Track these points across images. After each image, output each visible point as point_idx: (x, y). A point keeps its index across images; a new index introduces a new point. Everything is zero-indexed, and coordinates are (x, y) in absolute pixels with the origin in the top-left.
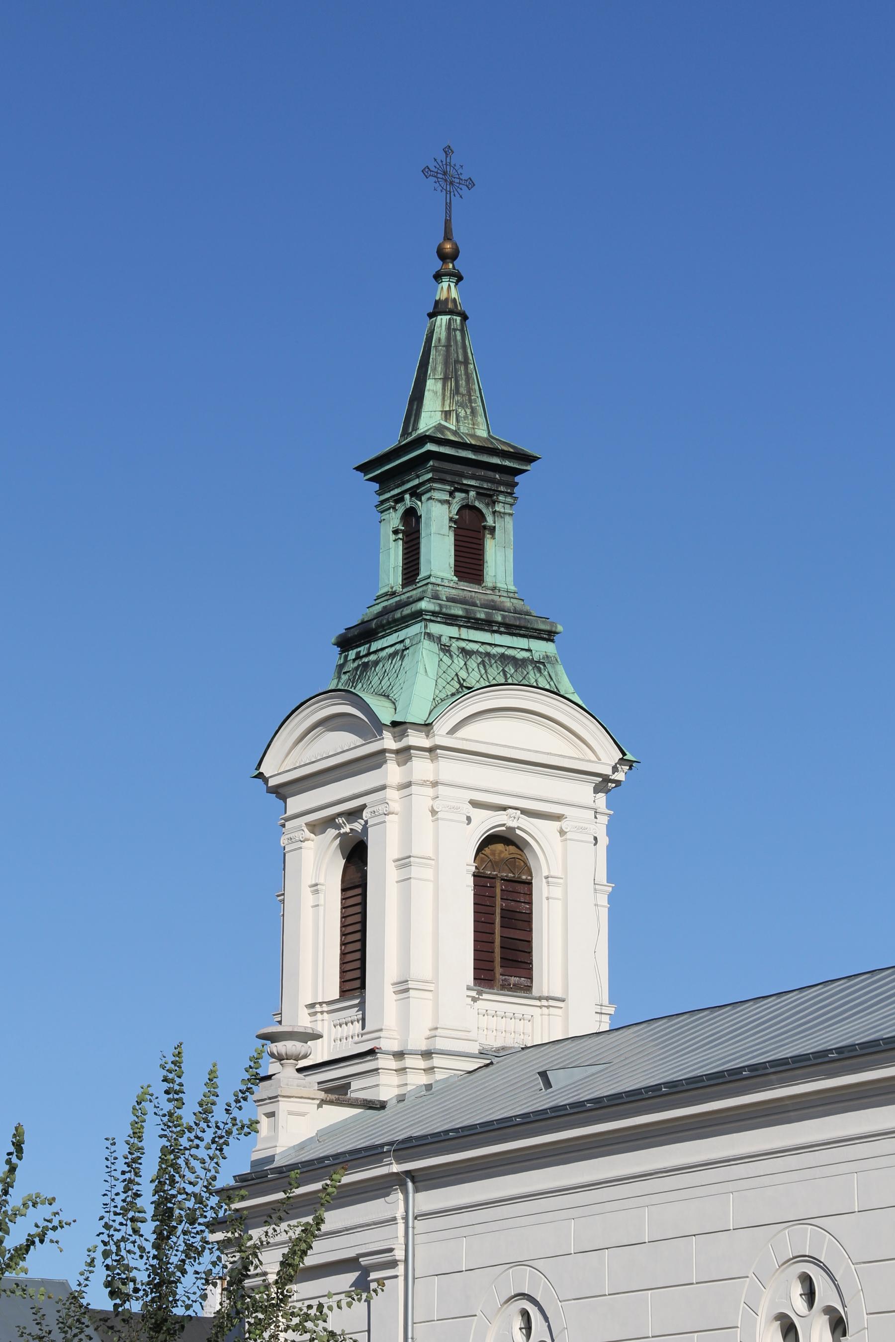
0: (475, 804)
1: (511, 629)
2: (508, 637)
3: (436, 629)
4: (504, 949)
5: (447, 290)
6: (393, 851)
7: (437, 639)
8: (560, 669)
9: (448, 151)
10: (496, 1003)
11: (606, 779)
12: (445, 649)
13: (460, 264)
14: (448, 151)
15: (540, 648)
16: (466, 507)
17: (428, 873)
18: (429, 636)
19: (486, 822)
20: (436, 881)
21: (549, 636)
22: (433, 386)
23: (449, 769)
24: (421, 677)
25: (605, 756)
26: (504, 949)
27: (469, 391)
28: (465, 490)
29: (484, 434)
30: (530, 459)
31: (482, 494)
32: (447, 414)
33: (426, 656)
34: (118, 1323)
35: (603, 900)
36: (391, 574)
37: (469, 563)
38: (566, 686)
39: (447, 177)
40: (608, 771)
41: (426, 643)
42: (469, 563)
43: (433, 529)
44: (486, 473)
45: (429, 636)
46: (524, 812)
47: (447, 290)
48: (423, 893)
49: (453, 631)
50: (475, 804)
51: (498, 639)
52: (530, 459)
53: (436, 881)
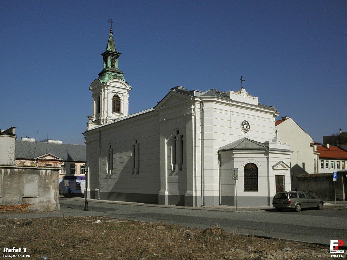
0: (113, 92)
1: (118, 73)
2: (117, 74)
3: (108, 72)
4: (116, 108)
5: (111, 34)
6: (103, 97)
7: (109, 74)
8: (124, 78)
9: (111, 19)
10: (114, 114)
11: (128, 89)
12: (109, 75)
13: (113, 32)
14: (111, 19)
15: (121, 75)
16: (113, 59)
17: (122, 102)
18: (108, 73)
19: (114, 94)
20: (123, 103)
21: (122, 74)
22: (109, 45)
23: (109, 88)
24: (106, 78)
25: (128, 87)
26: (116, 108)
27: (113, 46)
28: (113, 57)
29: (115, 51)
30: (120, 54)
31: (114, 58)
32: (110, 49)
33: (107, 75)
34: (341, 259)
35: (128, 103)
36: (105, 67)
37: (113, 66)
38: (124, 79)
39: (111, 22)
40: (128, 89)
41: (107, 74)
42: (113, 66)
43: (109, 61)
44: (116, 55)
45: (108, 73)
46: (118, 93)
47: (111, 34)
48: (106, 101)
49: (110, 73)
50: (113, 92)
51: (116, 74)
52: (120, 54)
53: (123, 103)
